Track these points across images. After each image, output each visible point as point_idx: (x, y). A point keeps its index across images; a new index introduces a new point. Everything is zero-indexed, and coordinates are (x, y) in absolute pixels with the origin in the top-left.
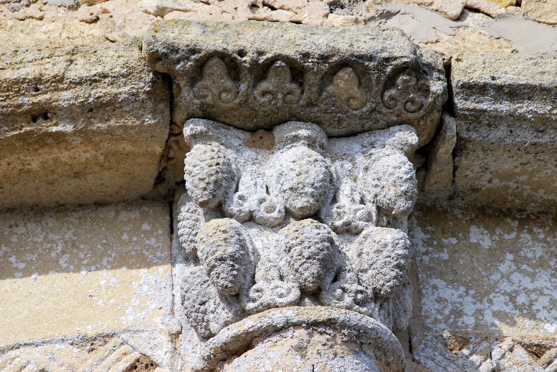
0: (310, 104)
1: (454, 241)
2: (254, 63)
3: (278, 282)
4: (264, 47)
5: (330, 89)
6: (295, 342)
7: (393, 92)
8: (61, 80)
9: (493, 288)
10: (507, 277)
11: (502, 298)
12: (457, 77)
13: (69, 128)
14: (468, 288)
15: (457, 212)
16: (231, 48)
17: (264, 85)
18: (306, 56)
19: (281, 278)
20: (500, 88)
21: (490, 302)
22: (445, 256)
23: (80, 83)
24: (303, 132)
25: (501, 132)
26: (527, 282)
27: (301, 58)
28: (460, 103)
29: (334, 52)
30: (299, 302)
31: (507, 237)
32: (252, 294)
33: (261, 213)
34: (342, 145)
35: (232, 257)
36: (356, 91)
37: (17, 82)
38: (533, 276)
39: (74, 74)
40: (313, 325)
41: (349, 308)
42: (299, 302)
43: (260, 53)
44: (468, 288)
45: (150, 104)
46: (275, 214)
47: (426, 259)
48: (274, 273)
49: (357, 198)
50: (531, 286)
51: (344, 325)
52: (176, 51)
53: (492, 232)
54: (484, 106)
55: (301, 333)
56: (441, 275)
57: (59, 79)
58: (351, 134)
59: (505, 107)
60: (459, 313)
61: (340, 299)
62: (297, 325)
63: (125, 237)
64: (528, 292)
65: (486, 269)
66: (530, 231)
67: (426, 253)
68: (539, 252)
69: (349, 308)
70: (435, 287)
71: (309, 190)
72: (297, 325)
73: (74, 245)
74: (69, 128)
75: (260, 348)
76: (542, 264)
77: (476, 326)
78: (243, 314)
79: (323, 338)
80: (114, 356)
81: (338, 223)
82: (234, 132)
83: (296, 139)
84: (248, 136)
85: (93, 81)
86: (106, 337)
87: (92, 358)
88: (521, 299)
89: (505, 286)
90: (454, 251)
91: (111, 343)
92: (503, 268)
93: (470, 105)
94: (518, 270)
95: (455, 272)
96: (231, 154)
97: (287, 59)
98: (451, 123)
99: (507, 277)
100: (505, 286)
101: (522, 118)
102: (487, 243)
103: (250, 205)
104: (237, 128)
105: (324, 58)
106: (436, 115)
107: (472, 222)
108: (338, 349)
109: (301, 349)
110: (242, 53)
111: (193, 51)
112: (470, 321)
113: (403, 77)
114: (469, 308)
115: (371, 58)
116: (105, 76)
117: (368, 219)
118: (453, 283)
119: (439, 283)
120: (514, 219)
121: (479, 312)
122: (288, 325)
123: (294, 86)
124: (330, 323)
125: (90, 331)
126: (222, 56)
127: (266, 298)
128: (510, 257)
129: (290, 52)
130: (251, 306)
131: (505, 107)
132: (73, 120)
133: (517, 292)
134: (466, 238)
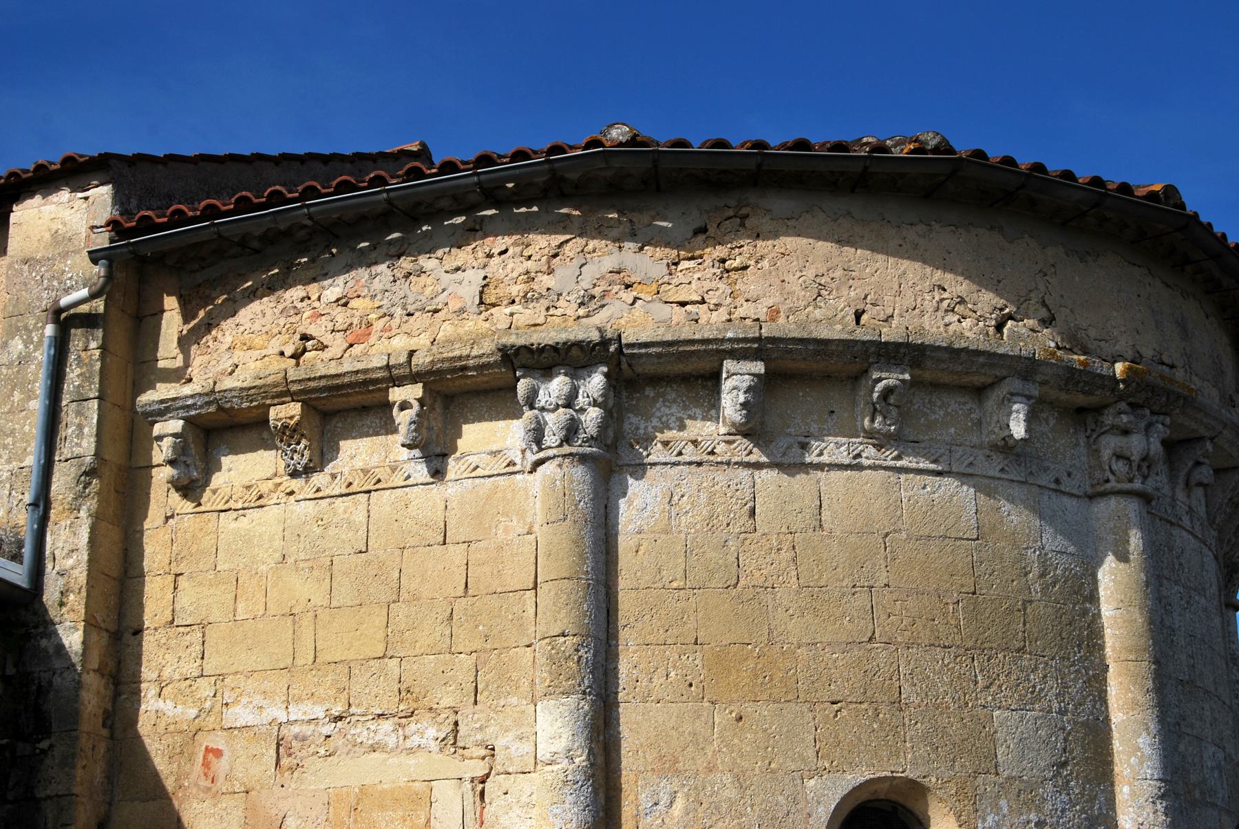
0: (563, 360)
1: (638, 395)
2: (537, 348)
3: (553, 437)
4: (541, 341)
5: (570, 354)
6: (558, 463)
7: (595, 353)
8: (469, 356)
9: (653, 415)
10: (659, 409)
11: (657, 420)
12: (623, 341)
13: (475, 373)
14: (642, 416)
15: (641, 381)
16: (527, 344)
17: (544, 355)
18: (557, 343)
19: (554, 435)
20: (640, 344)
21: (651, 422)
22: (634, 403)
23: (476, 357)
24: (562, 371)
25: (644, 359)
26: (667, 411)
27: (340, 701)
28: (625, 351)
29: (568, 341)
30: (560, 445)
31: (661, 390)
32: (544, 442)
33: (547, 407)
34: (580, 372)
35: (534, 429)
36: (580, 354)
37: (453, 358)
38: (670, 408)
39: (473, 354)
40: (564, 456)
41: (580, 446)
42: (560, 445)
43: (539, 344)
44: (642, 416)
45: (502, 364)
46: (552, 406)
47: (626, 405)
48: (551, 433)
49: (585, 395)
50: (668, 412)
51: (576, 454)
52: (506, 347)
53: (655, 389)
54: (635, 351)
55: (560, 459)
56: (632, 412)
57: (468, 356)
58: (583, 367)
59: (643, 351)
60: (637, 429)
61: (577, 442)
62: (558, 456)
63: (508, 404)
64: (667, 415)
65: (651, 406)
66: (671, 387)
67: (627, 402)
68: (674, 395)
69: (580, 446)
70: (629, 418)
71: (563, 397)
72: (558, 456)
73: (490, 408)
74: (475, 373)
75: (547, 464)
76: (674, 401)
77: (645, 434)
78: (541, 450)
79: (568, 460)
80: (502, 460)
81: (577, 408)
82: (537, 371)
83: (560, 373)
84: (543, 371)
85: (480, 356)
86: (500, 452)
87: (496, 459)
88: (664, 419)
89: (658, 414)
90: (638, 399)
91: (501, 454)
92: (658, 405)
93: (630, 351)
94: (664, 406)
95: (638, 410)
96: (535, 382)
97: (549, 345)
98: (624, 359)
99: (659, 409)
100: (658, 414)
101: (651, 354)
102: (652, 394)
103: (542, 404)
104: (538, 369)
105: (565, 343)
106: (616, 356)
107: (646, 385)
108: (575, 464)
109: (560, 466)
110: (532, 345)
111: (513, 346)
112: (642, 431)
113: (597, 348)
114: (642, 426)
115: (583, 342)
116: (484, 354)
117: (589, 404)
118: (636, 415)
119: (630, 415)
120: (665, 381)
121: (646, 427)
122: (555, 457)
123: (555, 354)
124: (571, 454)
125: (494, 449)
126: (525, 347)
127: (548, 444)
128: (661, 399)
129: (550, 343)
130: (543, 447)
131: (643, 351)
132: (476, 371)
133: (662, 416)
134: (644, 393)
